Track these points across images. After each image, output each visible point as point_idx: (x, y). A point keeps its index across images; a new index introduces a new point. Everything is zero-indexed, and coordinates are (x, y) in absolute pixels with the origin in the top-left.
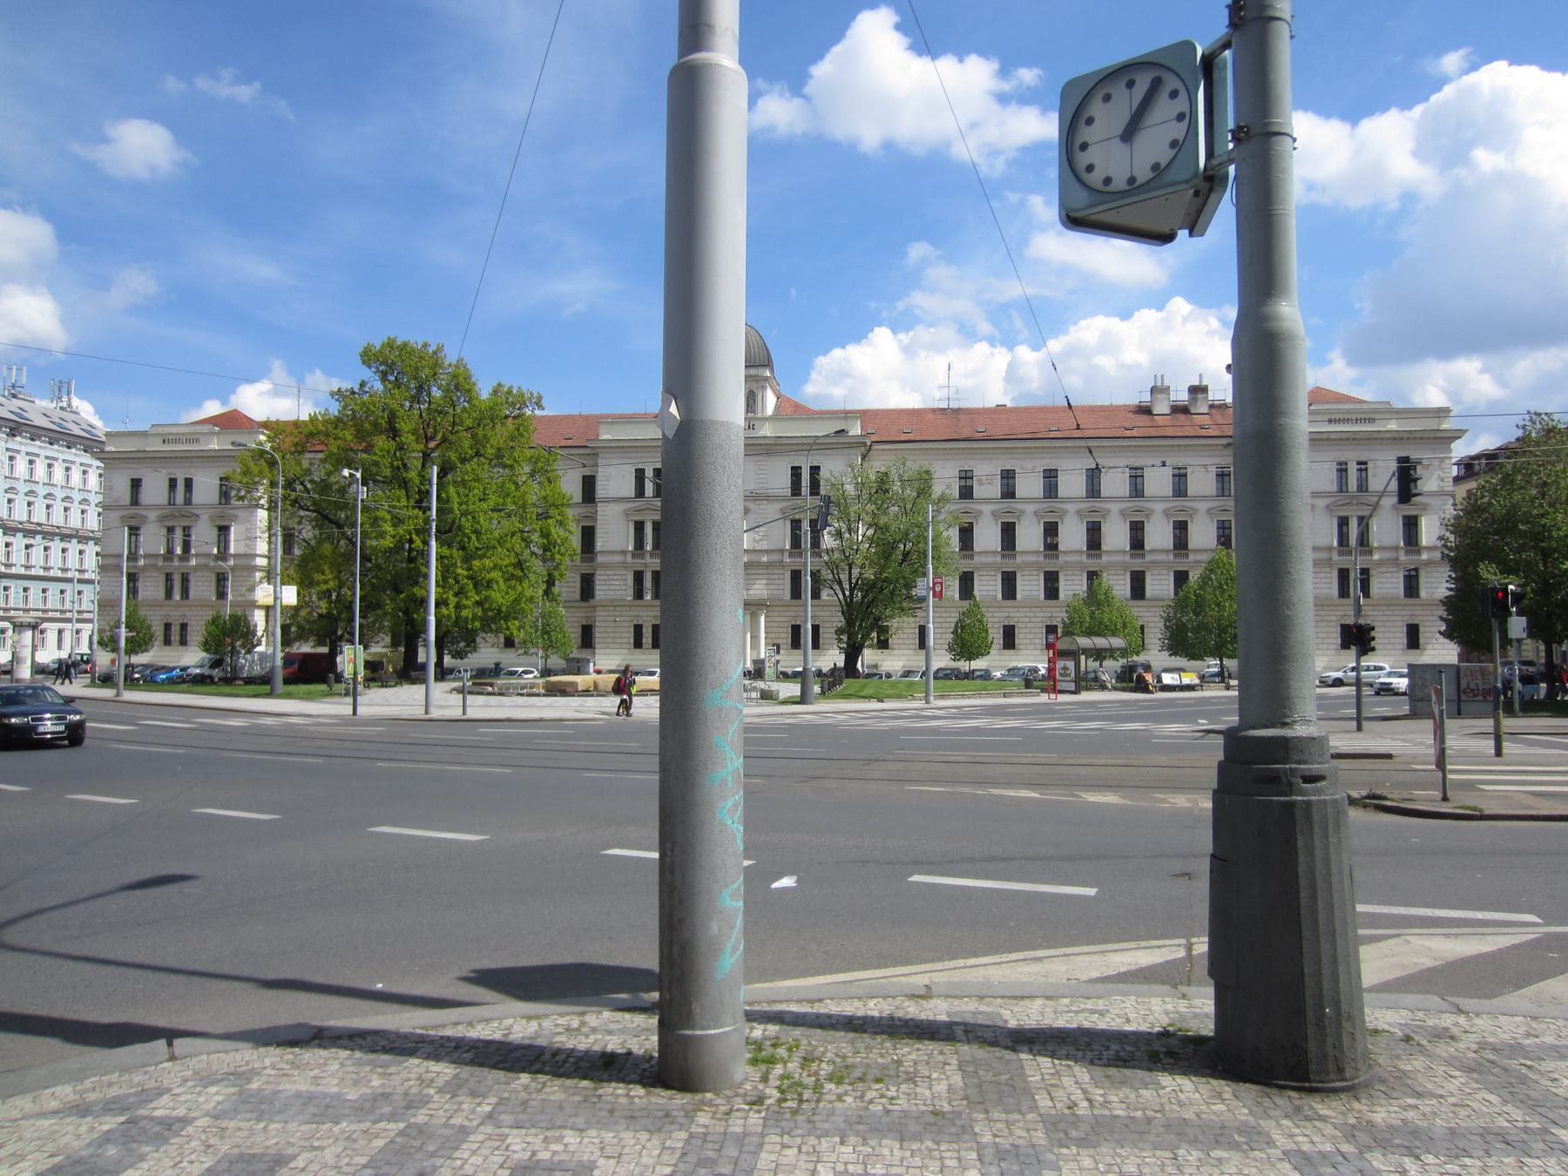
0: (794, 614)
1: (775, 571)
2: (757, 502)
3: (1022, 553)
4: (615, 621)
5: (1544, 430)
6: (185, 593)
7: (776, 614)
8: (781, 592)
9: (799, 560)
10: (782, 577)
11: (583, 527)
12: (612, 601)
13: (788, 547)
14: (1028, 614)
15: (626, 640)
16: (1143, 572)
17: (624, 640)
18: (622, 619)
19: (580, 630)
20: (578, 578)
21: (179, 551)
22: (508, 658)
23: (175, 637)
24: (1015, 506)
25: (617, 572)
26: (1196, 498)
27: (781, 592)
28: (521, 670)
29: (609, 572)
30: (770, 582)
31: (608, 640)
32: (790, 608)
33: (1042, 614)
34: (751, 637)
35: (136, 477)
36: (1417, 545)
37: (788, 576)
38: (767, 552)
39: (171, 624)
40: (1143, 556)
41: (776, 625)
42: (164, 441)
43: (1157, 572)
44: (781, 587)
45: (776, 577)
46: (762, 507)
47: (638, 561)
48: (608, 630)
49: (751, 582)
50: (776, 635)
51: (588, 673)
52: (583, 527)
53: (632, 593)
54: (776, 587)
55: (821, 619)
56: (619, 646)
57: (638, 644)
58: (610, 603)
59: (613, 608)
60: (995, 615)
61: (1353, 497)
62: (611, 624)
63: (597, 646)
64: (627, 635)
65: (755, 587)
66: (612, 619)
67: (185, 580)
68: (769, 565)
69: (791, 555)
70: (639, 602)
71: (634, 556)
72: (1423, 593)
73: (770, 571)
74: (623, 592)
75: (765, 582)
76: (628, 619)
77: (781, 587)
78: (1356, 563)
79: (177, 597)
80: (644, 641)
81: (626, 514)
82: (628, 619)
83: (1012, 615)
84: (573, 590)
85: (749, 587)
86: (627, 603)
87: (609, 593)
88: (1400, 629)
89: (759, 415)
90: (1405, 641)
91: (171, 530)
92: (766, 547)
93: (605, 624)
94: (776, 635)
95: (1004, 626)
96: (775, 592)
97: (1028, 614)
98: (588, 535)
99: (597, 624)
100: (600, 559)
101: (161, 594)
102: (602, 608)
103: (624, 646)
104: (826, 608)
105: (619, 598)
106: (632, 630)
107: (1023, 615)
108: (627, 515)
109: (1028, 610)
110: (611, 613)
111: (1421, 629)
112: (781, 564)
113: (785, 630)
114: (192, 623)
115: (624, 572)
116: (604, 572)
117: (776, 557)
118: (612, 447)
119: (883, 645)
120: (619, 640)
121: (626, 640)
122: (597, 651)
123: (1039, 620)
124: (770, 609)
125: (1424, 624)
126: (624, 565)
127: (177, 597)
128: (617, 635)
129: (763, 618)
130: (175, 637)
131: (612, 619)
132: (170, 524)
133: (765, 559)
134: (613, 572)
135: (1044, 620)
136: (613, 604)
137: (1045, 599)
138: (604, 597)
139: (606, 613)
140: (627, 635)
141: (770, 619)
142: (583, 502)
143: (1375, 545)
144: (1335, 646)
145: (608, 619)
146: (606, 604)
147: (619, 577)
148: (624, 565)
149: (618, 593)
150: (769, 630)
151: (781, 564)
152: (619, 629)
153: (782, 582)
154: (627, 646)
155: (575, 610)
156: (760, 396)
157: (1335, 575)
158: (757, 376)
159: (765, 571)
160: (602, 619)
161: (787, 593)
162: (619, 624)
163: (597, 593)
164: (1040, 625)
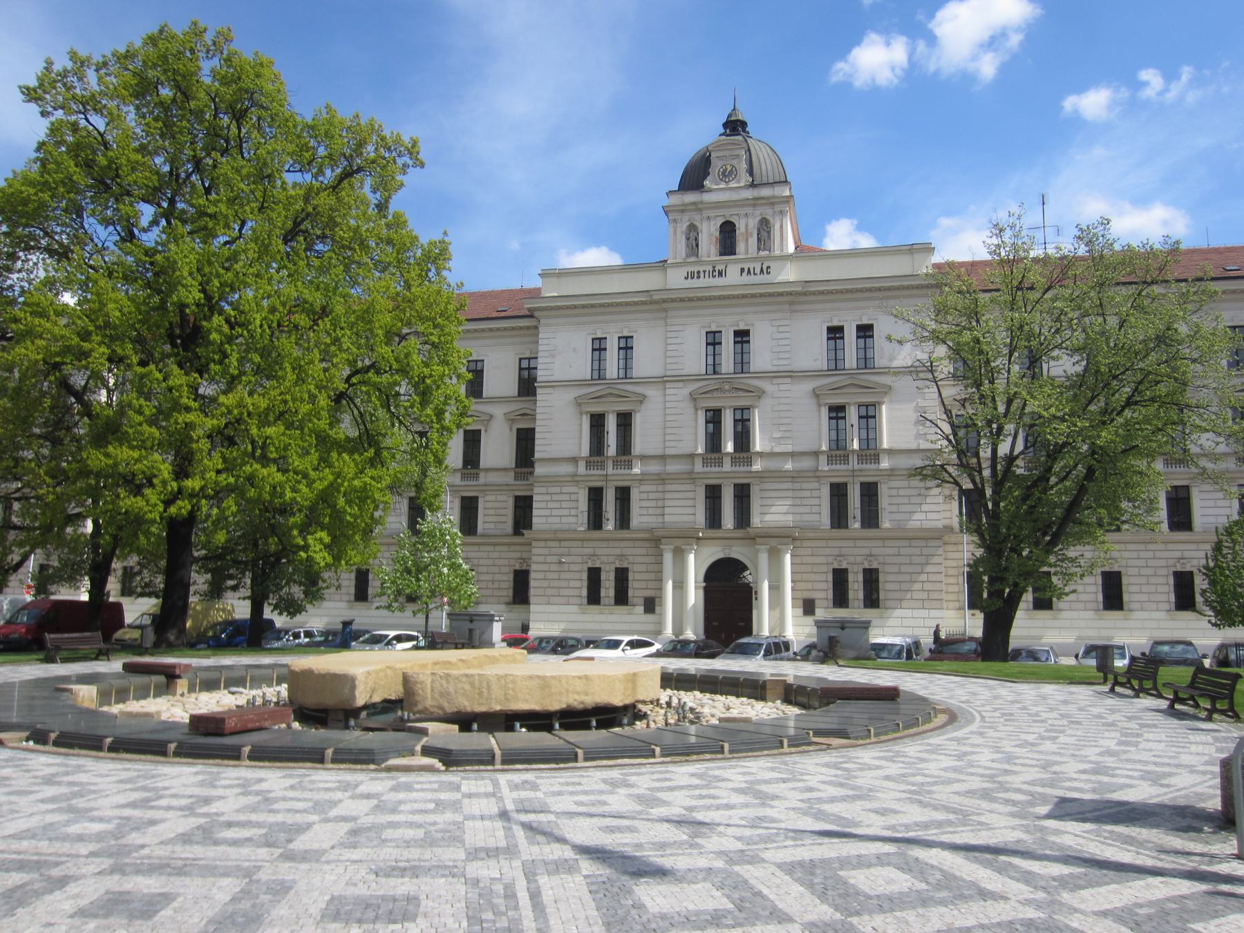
0: (836, 552)
1: (805, 486)
2: (775, 381)
3: (487, 470)
4: (560, 562)
5: (45, 362)
6: (624, 520)
7: (809, 552)
8: (816, 517)
9: (843, 467)
10: (815, 493)
11: (519, 430)
12: (555, 531)
13: (700, 450)
14: (1143, 554)
15: (576, 592)
16: (1187, 488)
17: (571, 592)
18: (570, 559)
19: (511, 577)
20: (510, 503)
21: (729, 447)
22: (363, 616)
23: (608, 589)
24: (481, 408)
25: (565, 490)
26: (494, 400)
27: (816, 517)
28: (392, 634)
29: (551, 490)
30: (798, 502)
31: (549, 592)
32: (831, 543)
33: (1166, 554)
34: (770, 588)
35: (865, 321)
36: (748, 450)
37: (826, 492)
38: (793, 455)
39: (845, 571)
40: (476, 476)
41: (809, 568)
42: (742, 270)
43: (493, 498)
44: (815, 509)
45: (807, 494)
46: (782, 387)
47: (595, 472)
48: (550, 576)
49: (766, 502)
50: (809, 586)
51: (490, 645)
52: (519, 430)
53: (586, 521)
54: (807, 509)
55: (881, 559)
56: (564, 600)
57: (594, 597)
58: (552, 536)
59: (556, 544)
60: (1159, 554)
61: (728, 380)
62: (554, 567)
63: (532, 599)
64: (577, 584)
65: (774, 509)
66: (555, 559)
67: (623, 495)
68: (795, 476)
69: (706, 462)
70: (596, 534)
71: (589, 465)
72: (886, 524)
73: (797, 486)
74: (573, 520)
75: (789, 502)
76: (579, 559)
77: (815, 509)
78: (611, 477)
79: (610, 525)
80: (603, 593)
81: (578, 402)
82: (579, 559)
83: (1187, 554)
84: (503, 519)
85: (766, 510)
86: (581, 536)
87: (550, 520)
88: (823, 577)
89: (777, 253)
90: (1172, 598)
91: (837, 412)
92: (789, 448)
93: (545, 567)
94: (809, 586)
95: (865, 570)
96: (807, 518)
97: (491, 555)
98: (525, 441)
99: (533, 567)
100: (539, 470)
101: (700, 518)
102: (542, 544)
103: (572, 600)
104: (888, 543)
105: (566, 527)
106: (585, 576)
107: (485, 555)
108: (579, 405)
109: (1142, 547)
110: (554, 551)
111: (1125, 580)
112: (815, 475)
113: (577, 576)
114: (888, 569)
115: (573, 489)
116: (543, 490)
117: (807, 463)
118: (559, 308)
119: (1043, 604)
120: (566, 592)
121: (576, 592)
122: (533, 608)
123: (1163, 563)
124: (798, 543)
125: (888, 569)
126: (574, 479)
127: (610, 525)
128: (564, 584)
129: (691, 558)
130: (608, 589)
131: (555, 559)
132: (838, 400)
133: (789, 466)
134: (557, 490)
135: (512, 562)
136: (557, 537)
137: (833, 527)
138: (545, 527)
139: (546, 551)
140: (577, 584)
141: (798, 560)
142: (519, 395)
143: (885, 445)
144: (1166, 606)
145: (549, 559)
146: (547, 536)
147: (567, 497)
148: (574, 479)
149: (564, 520)
150: (798, 577)
151: (815, 475)
152: (567, 575)
153: (816, 501)
154: (577, 600)
155: (505, 548)
156: (777, 226)
157: (701, 494)
158: (773, 197)
159: (789, 485)
160: (541, 559)
161: (824, 517)
162: (566, 567)
163: (535, 520)
164: (1164, 571)
